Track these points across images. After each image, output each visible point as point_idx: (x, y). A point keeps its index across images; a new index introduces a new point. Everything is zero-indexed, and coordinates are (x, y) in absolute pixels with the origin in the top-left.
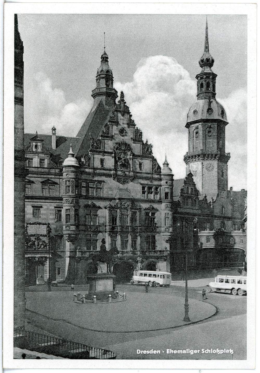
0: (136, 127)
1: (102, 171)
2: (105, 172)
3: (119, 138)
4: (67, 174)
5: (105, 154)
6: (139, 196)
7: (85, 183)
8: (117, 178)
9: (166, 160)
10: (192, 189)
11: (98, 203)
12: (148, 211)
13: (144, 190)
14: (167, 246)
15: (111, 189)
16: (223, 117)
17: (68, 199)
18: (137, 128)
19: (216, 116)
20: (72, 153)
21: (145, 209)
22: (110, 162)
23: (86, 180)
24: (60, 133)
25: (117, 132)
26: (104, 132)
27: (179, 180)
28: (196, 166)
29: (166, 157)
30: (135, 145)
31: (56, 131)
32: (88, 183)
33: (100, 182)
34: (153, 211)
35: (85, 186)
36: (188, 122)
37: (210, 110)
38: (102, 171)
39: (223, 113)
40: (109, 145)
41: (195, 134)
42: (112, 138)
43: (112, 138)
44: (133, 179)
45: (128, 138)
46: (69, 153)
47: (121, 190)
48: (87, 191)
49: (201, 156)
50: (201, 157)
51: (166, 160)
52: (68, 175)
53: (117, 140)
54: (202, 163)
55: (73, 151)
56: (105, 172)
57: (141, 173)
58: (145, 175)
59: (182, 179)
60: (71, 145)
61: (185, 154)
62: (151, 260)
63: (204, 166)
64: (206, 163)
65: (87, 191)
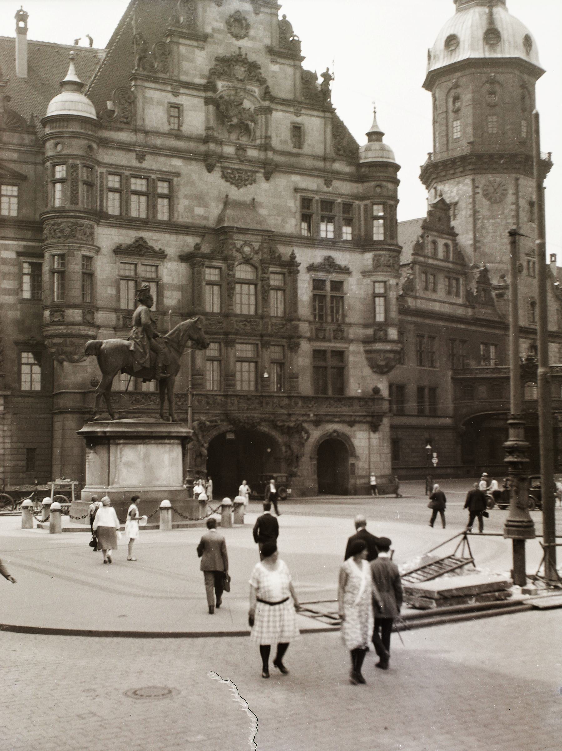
0: (280, 13)
1: (173, 143)
2: (181, 144)
3: (225, 46)
4: (56, 145)
5: (182, 90)
6: (292, 225)
7: (117, 178)
8: (222, 167)
9: (375, 125)
10: (446, 245)
11: (156, 239)
12: (321, 275)
13: (309, 208)
14: (380, 386)
15: (200, 199)
16: (528, 52)
17: (61, 223)
18: (284, 17)
19: (509, 50)
20: (77, 79)
21: (311, 268)
22: (196, 117)
23: (115, 170)
24: (33, 35)
25: (221, 25)
26: (178, 21)
27: (411, 222)
28: (456, 190)
29: (375, 112)
30: (275, 68)
31: (29, 20)
32: (128, 179)
33: (168, 178)
34: (335, 277)
35: (117, 185)
36: (432, 69)
37: (492, 35)
38: (173, 143)
39: (528, 41)
40: (196, 62)
41: (451, 100)
42: (203, 39)
43: (203, 39)
44: (270, 170)
45: (255, 45)
46: (67, 79)
47: (227, 203)
48: (125, 204)
49: (469, 161)
50: (470, 163)
51: (375, 125)
52: (59, 147)
53: (221, 51)
54: (473, 180)
55: (78, 73)
56: (181, 144)
57: (298, 155)
58: (309, 163)
59: (417, 221)
60: (71, 57)
61: (423, 160)
62: (331, 427)
63: (478, 187)
64: (482, 180)
65: (125, 204)
